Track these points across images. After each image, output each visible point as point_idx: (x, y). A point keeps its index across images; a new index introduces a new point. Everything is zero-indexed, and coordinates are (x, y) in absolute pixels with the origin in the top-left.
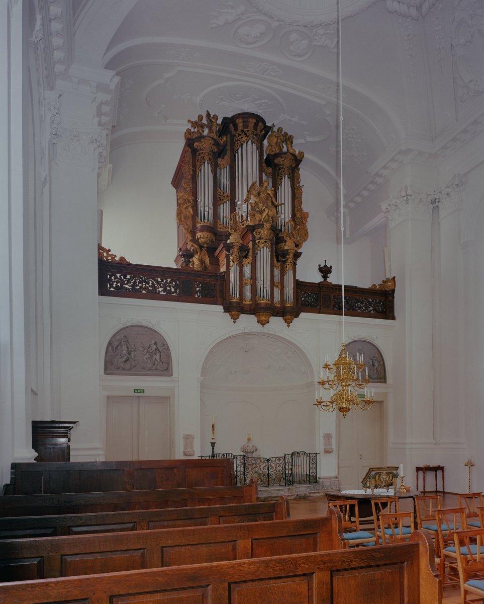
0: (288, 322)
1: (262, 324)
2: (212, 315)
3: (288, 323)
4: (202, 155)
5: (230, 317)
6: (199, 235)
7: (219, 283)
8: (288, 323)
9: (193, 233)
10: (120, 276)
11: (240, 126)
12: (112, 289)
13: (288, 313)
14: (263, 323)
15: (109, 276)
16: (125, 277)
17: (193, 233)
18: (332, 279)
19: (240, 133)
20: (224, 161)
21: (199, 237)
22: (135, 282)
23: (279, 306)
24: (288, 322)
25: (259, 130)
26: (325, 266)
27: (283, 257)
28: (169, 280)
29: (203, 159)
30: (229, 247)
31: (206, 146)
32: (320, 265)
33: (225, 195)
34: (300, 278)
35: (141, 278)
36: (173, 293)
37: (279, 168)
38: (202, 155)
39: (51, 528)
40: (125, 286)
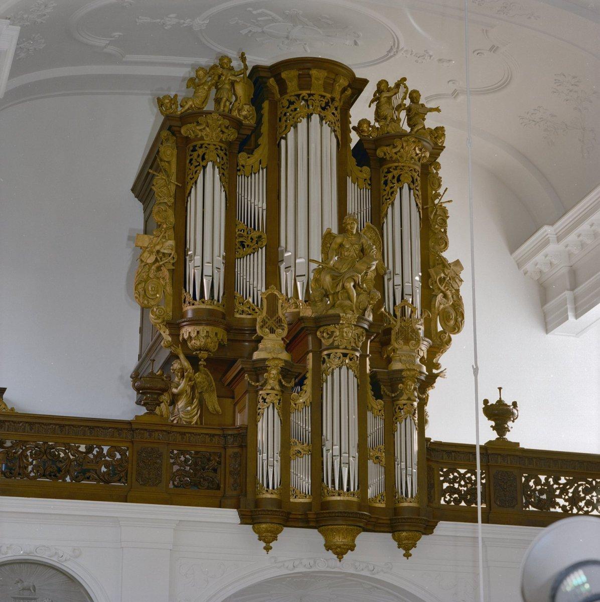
0: (407, 547)
1: (336, 553)
2: (212, 531)
4: (201, 152)
5: (256, 536)
6: (187, 331)
7: (230, 451)
9: (174, 326)
11: (292, 86)
13: (406, 524)
14: (340, 552)
15: (523, 479)
16: (556, 481)
17: (174, 326)
18: (526, 434)
19: (293, 99)
20: (253, 160)
21: (186, 337)
22: (576, 492)
23: (383, 505)
24: (407, 547)
25: (338, 89)
26: (500, 402)
27: (394, 390)
28: (106, 449)
29: (203, 159)
30: (259, 369)
31: (210, 133)
33: (255, 235)
34: (434, 433)
35: (588, 482)
37: (389, 169)
38: (201, 152)
39: (444, 193)
40: (558, 500)
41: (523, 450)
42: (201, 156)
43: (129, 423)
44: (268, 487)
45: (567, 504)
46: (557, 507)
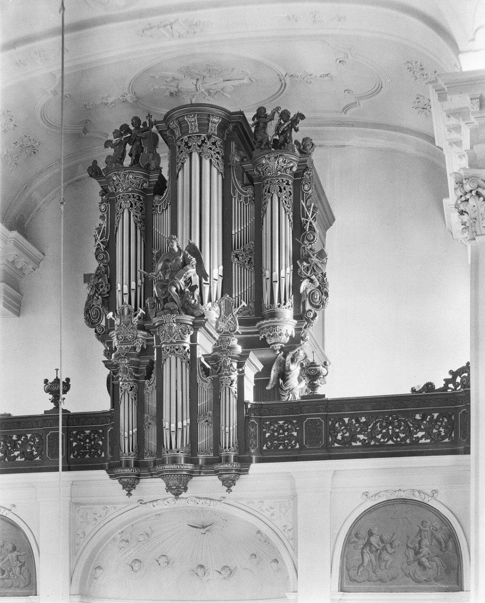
3: (229, 487)
8: (229, 487)
10: (349, 420)
12: (336, 445)
16: (358, 421)
22: (374, 428)
32: (46, 381)
36: (443, 438)
37: (267, 181)
40: (358, 436)
41: (328, 401)
42: (267, 191)
43: (41, 416)
44: (171, 447)
45: (366, 438)
46: (358, 442)
